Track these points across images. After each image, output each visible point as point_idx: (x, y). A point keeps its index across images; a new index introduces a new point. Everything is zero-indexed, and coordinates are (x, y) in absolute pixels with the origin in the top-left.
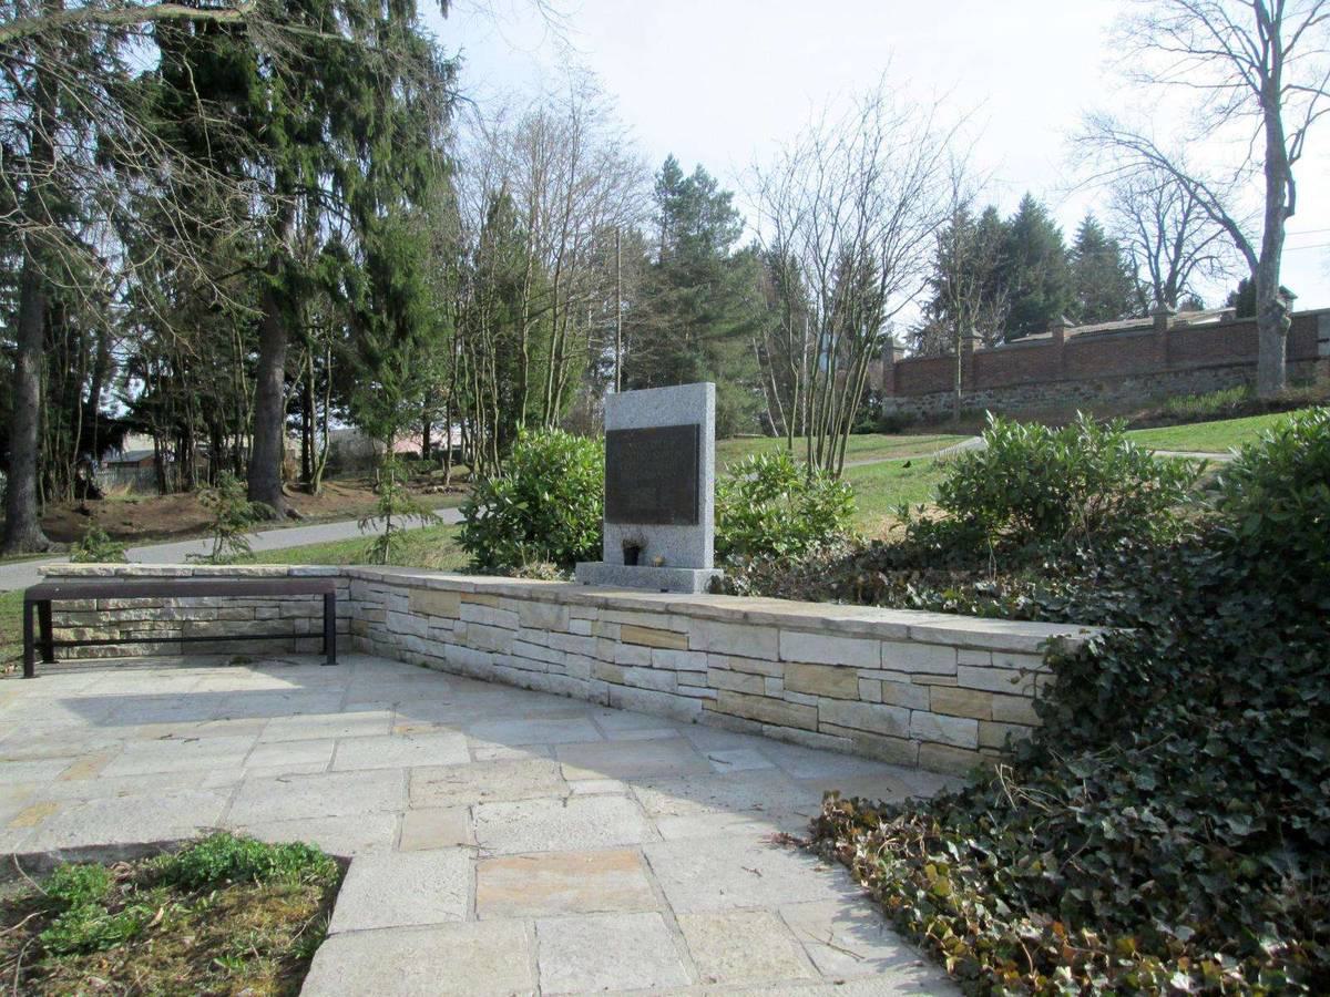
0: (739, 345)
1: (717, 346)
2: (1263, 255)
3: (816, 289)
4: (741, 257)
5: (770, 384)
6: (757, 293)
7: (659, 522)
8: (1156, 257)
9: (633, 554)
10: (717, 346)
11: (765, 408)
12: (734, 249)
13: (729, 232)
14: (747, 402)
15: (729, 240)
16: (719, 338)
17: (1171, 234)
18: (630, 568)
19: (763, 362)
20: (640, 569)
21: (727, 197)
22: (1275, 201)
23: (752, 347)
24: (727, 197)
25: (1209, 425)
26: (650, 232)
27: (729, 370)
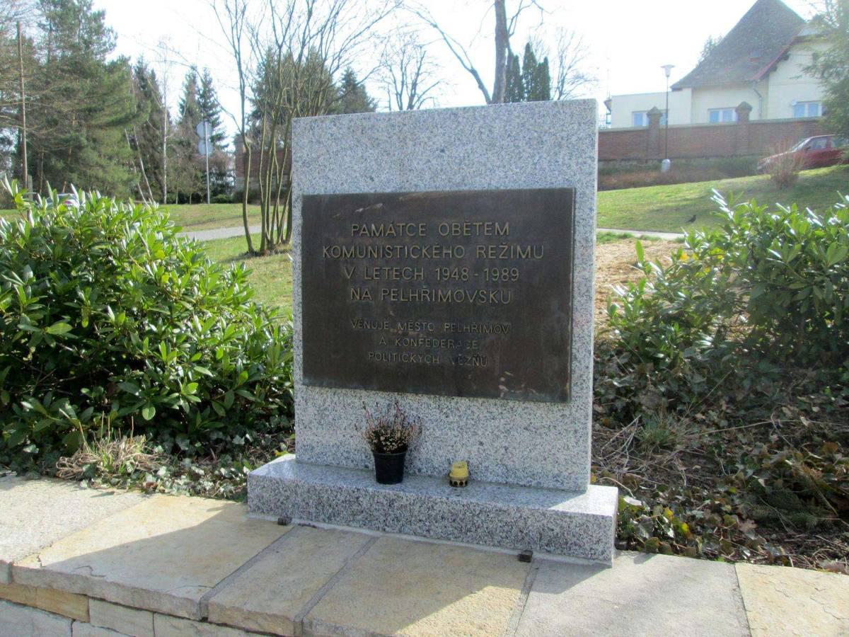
0: (116, 134)
1: (100, 133)
2: (494, 95)
3: (173, 101)
4: (113, 67)
5: (138, 165)
6: (130, 91)
7: (461, 391)
8: (401, 95)
9: (391, 460)
10: (100, 133)
11: (137, 182)
12: (110, 58)
13: (104, 44)
14: (126, 177)
15: (105, 51)
16: (101, 127)
17: (409, 81)
18: (388, 491)
19: (134, 147)
20: (404, 493)
21: (101, 15)
22: (501, 61)
23: (124, 136)
24: (101, 15)
25: (228, 205)
26: (35, 34)
27: (109, 151)
